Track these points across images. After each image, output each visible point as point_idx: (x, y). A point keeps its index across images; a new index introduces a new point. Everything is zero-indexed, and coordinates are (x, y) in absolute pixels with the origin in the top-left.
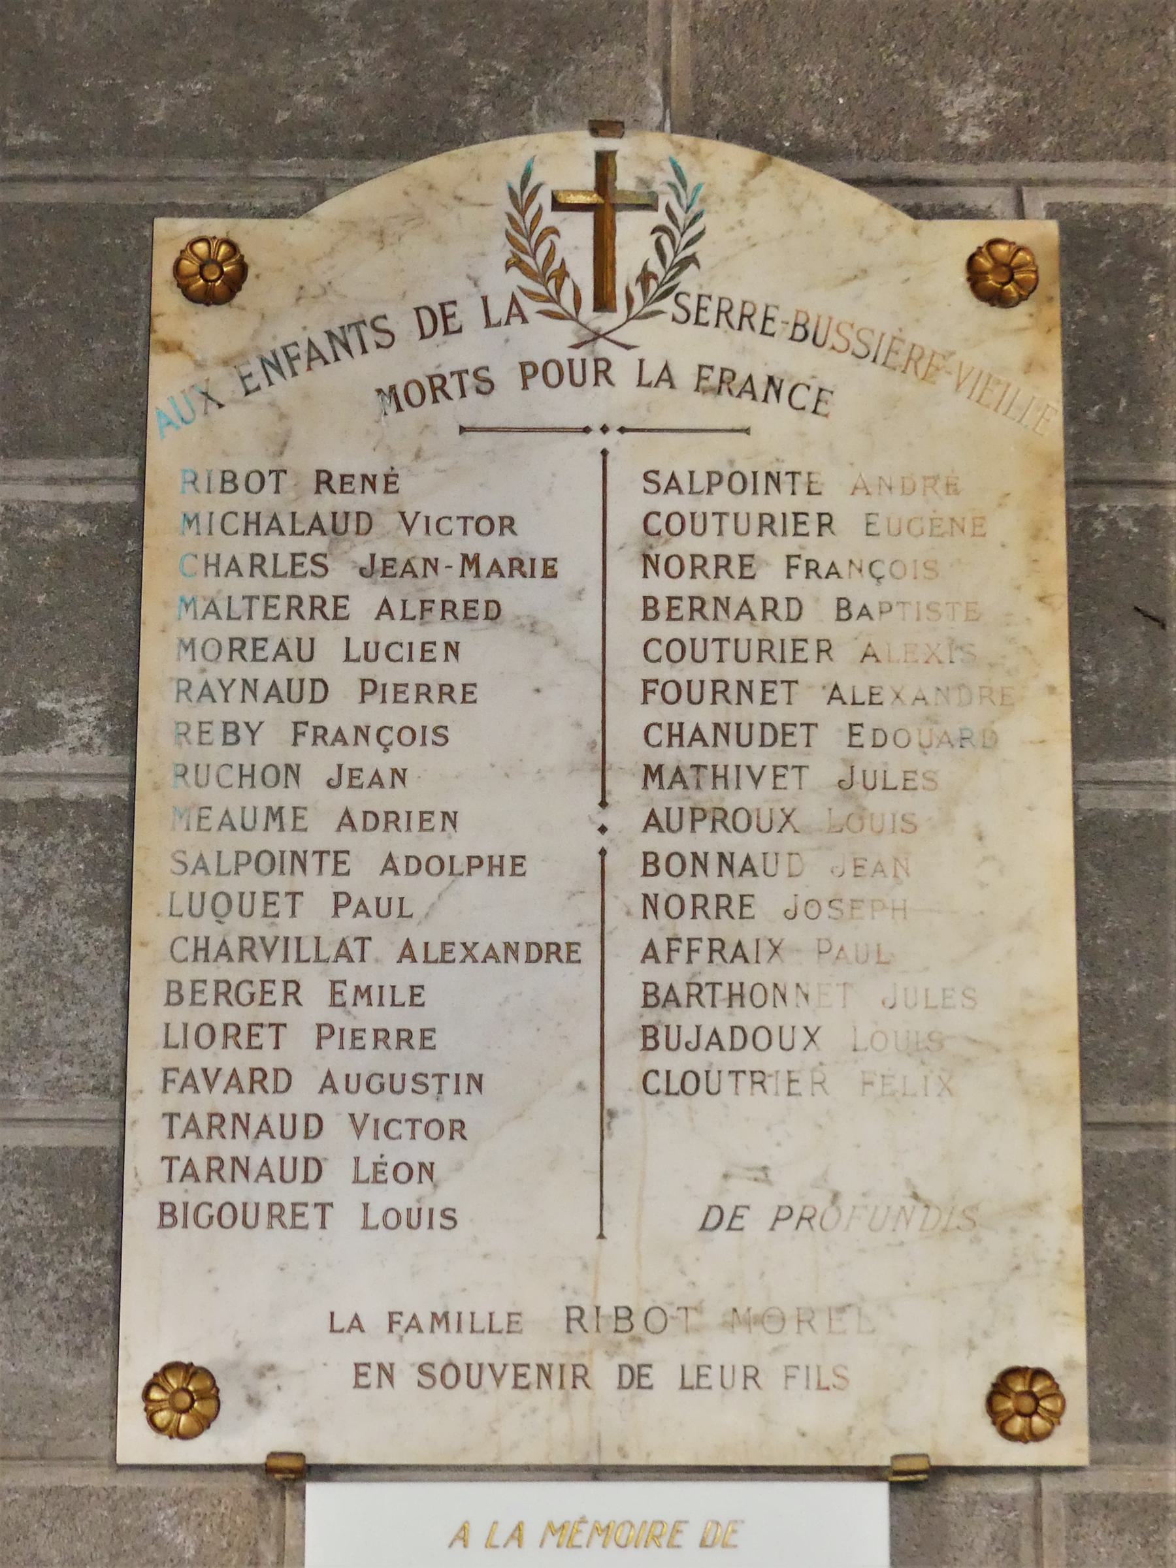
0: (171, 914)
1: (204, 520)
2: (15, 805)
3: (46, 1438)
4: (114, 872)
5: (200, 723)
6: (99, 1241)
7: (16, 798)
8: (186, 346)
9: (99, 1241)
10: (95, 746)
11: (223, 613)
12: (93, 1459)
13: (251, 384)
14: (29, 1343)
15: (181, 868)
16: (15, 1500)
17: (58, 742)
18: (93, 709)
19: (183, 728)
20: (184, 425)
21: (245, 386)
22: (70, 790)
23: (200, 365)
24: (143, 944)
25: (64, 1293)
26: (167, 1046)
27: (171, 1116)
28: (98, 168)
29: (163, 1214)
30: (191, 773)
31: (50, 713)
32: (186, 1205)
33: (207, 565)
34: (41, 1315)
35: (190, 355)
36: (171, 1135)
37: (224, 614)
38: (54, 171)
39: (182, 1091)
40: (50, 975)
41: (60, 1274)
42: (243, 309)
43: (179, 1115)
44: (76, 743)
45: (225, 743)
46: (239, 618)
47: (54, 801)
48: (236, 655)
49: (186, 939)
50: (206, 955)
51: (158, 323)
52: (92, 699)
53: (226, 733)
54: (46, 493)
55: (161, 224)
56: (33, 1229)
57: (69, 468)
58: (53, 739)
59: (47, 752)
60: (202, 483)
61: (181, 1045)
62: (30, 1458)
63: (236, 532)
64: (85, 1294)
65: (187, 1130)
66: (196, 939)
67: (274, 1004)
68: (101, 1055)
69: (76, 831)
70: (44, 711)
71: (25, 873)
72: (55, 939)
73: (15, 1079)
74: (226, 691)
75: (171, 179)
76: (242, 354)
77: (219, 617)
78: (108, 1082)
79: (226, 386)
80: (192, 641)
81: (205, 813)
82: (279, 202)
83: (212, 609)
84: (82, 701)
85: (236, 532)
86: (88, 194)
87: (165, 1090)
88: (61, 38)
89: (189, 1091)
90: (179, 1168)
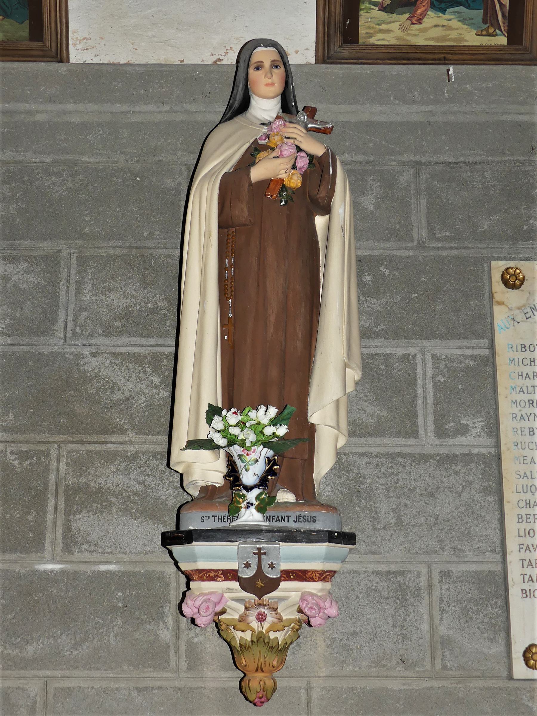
0: (517, 492)
1: (516, 360)
2: (457, 455)
3: (484, 670)
4: (492, 478)
5: (521, 428)
6: (496, 603)
7: (457, 453)
8: (505, 303)
9: (496, 603)
10: (482, 436)
11: (525, 391)
12: (500, 677)
13: (528, 316)
14: (475, 637)
15: (519, 477)
16: (475, 692)
17: (469, 434)
18: (480, 423)
19: (515, 430)
20: (507, 329)
21: (526, 317)
22: (475, 451)
23: (510, 309)
24: (509, 502)
25: (486, 620)
26: (519, 536)
27: (522, 560)
28: (466, 244)
29: (523, 593)
30: (519, 444)
31: (466, 424)
32: (530, 590)
33: (519, 375)
34: (478, 628)
35: (507, 306)
36: (523, 567)
37: (526, 392)
38: (452, 245)
39: (525, 552)
40: (473, 512)
41: (484, 614)
42: (523, 291)
43: (525, 560)
44: (475, 435)
45: (530, 435)
46: (531, 393)
47: (469, 454)
48: (531, 405)
49: (522, 500)
50: (530, 506)
51: (495, 295)
52: (479, 420)
53: (530, 431)
54: (458, 351)
55: (493, 263)
56: (474, 598)
57: (466, 343)
58: (467, 433)
59: (466, 437)
60: (514, 348)
61: (524, 536)
62: (479, 677)
63: (527, 365)
64: (493, 621)
65: (528, 565)
66: (526, 500)
67: (530, 522)
68: (492, 540)
69: (478, 464)
70: (464, 424)
71: (462, 478)
72: (473, 500)
73: (464, 547)
74: (529, 418)
75: (490, 248)
76: (524, 306)
77: (524, 393)
78: (495, 549)
79: (520, 316)
80: (516, 401)
81: (525, 458)
82: (527, 256)
83: (521, 390)
84: (476, 421)
85: (527, 365)
86: (464, 252)
87: (520, 551)
88: (450, 202)
89: (528, 551)
90: (527, 578)
